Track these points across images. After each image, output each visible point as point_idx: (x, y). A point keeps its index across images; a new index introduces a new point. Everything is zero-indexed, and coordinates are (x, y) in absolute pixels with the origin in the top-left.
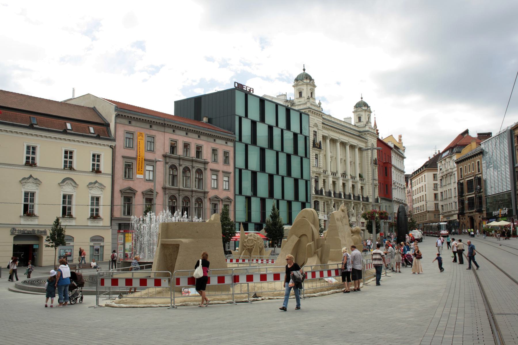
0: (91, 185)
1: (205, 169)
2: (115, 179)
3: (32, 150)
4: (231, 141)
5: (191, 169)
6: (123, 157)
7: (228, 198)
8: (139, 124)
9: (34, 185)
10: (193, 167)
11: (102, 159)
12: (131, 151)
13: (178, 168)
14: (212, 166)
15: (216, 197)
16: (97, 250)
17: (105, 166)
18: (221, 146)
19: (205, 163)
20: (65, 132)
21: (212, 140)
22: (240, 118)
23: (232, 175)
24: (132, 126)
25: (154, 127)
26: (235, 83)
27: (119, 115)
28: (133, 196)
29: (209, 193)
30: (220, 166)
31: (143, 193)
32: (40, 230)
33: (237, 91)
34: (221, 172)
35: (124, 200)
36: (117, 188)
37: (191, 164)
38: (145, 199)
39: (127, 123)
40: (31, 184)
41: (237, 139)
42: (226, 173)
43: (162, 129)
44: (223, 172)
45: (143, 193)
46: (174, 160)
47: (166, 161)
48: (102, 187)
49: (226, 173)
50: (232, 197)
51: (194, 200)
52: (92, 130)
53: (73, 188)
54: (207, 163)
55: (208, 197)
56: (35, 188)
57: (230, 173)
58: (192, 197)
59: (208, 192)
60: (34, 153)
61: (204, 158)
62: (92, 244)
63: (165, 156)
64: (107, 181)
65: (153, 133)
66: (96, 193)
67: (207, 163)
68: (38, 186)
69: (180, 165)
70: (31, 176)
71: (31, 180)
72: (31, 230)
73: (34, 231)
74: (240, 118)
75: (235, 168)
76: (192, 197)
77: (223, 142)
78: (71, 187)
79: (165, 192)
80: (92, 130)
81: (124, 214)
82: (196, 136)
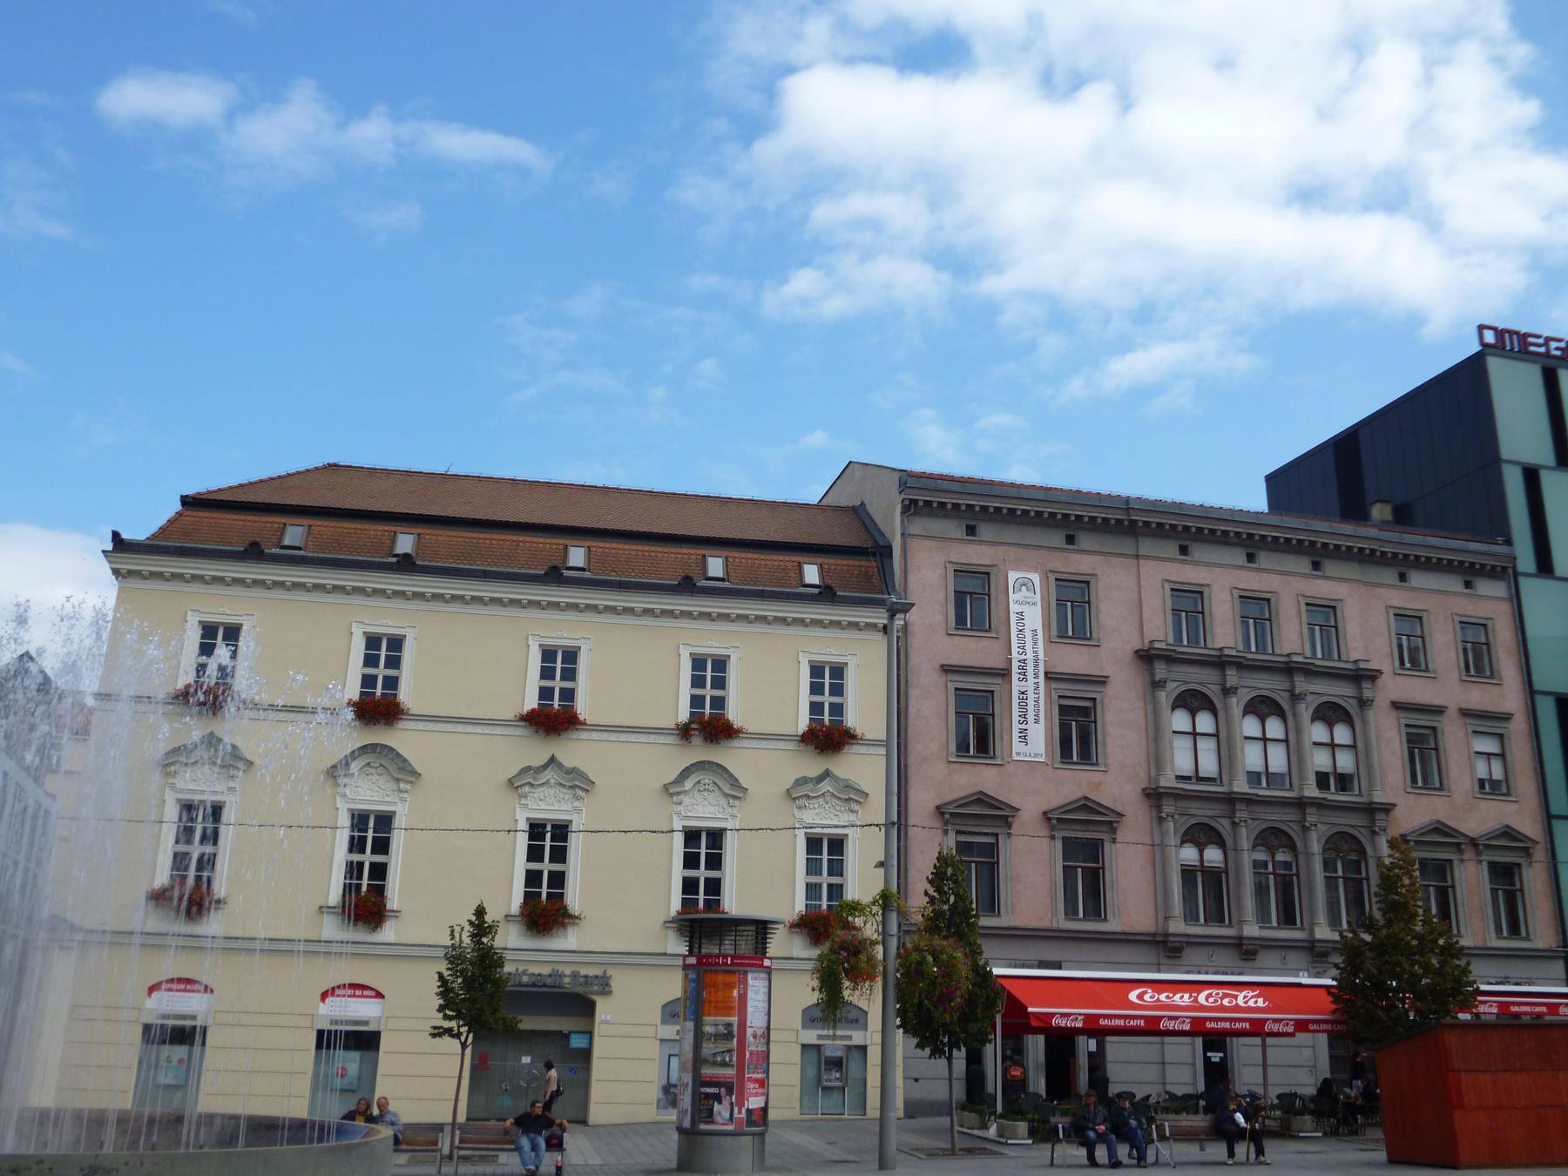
0: (799, 792)
1: (1364, 704)
2: (913, 759)
3: (560, 662)
4: (1495, 573)
5: (1285, 705)
6: (947, 669)
7: (1508, 833)
8: (1012, 534)
9: (566, 794)
10: (1296, 698)
11: (851, 681)
12: (985, 642)
13: (1219, 706)
14: (1395, 686)
15: (1440, 829)
16: (836, 1064)
17: (864, 709)
18: (1442, 603)
19: (1361, 676)
20: (555, 575)
21: (1389, 576)
22: (1531, 476)
23: (1519, 725)
24: (981, 542)
25: (1085, 541)
26: (1481, 328)
27: (914, 502)
28: (1524, 865)
29: (1397, 813)
30: (1445, 686)
31: (1047, 817)
32: (583, 972)
33: (1494, 364)
34: (1452, 712)
35: (1067, 855)
36: (923, 800)
37: (1286, 685)
38: (1059, 845)
39: (960, 533)
40: (552, 792)
41: (1526, 559)
42: (1486, 720)
43: (1127, 545)
44: (1466, 713)
45: (1047, 817)
46: (1195, 669)
47: (1152, 674)
48: (852, 795)
49: (1486, 720)
50: (1529, 825)
51: (1316, 847)
52: (812, 574)
53: (723, 802)
54: (1373, 676)
55: (1395, 832)
56: (220, 787)
57: (1506, 717)
58: (1305, 829)
59: (1387, 809)
60: (569, 674)
61: (1354, 657)
62: (811, 1036)
63: (1147, 657)
64: (865, 768)
65: (1078, 564)
66: (824, 817)
67: (1373, 676)
68: (577, 798)
69: (1227, 691)
70: (552, 760)
71: (549, 775)
72: (545, 970)
73: (556, 975)
74: (1531, 476)
75: (1531, 692)
76: (1374, 833)
77: (1454, 583)
78: (714, 797)
79: (1159, 808)
80: (812, 574)
81: (1071, 911)
82: (1304, 565)
